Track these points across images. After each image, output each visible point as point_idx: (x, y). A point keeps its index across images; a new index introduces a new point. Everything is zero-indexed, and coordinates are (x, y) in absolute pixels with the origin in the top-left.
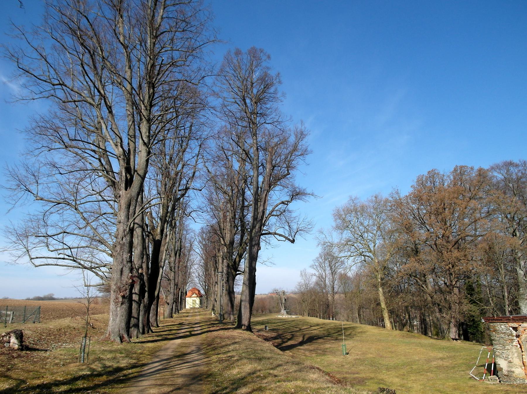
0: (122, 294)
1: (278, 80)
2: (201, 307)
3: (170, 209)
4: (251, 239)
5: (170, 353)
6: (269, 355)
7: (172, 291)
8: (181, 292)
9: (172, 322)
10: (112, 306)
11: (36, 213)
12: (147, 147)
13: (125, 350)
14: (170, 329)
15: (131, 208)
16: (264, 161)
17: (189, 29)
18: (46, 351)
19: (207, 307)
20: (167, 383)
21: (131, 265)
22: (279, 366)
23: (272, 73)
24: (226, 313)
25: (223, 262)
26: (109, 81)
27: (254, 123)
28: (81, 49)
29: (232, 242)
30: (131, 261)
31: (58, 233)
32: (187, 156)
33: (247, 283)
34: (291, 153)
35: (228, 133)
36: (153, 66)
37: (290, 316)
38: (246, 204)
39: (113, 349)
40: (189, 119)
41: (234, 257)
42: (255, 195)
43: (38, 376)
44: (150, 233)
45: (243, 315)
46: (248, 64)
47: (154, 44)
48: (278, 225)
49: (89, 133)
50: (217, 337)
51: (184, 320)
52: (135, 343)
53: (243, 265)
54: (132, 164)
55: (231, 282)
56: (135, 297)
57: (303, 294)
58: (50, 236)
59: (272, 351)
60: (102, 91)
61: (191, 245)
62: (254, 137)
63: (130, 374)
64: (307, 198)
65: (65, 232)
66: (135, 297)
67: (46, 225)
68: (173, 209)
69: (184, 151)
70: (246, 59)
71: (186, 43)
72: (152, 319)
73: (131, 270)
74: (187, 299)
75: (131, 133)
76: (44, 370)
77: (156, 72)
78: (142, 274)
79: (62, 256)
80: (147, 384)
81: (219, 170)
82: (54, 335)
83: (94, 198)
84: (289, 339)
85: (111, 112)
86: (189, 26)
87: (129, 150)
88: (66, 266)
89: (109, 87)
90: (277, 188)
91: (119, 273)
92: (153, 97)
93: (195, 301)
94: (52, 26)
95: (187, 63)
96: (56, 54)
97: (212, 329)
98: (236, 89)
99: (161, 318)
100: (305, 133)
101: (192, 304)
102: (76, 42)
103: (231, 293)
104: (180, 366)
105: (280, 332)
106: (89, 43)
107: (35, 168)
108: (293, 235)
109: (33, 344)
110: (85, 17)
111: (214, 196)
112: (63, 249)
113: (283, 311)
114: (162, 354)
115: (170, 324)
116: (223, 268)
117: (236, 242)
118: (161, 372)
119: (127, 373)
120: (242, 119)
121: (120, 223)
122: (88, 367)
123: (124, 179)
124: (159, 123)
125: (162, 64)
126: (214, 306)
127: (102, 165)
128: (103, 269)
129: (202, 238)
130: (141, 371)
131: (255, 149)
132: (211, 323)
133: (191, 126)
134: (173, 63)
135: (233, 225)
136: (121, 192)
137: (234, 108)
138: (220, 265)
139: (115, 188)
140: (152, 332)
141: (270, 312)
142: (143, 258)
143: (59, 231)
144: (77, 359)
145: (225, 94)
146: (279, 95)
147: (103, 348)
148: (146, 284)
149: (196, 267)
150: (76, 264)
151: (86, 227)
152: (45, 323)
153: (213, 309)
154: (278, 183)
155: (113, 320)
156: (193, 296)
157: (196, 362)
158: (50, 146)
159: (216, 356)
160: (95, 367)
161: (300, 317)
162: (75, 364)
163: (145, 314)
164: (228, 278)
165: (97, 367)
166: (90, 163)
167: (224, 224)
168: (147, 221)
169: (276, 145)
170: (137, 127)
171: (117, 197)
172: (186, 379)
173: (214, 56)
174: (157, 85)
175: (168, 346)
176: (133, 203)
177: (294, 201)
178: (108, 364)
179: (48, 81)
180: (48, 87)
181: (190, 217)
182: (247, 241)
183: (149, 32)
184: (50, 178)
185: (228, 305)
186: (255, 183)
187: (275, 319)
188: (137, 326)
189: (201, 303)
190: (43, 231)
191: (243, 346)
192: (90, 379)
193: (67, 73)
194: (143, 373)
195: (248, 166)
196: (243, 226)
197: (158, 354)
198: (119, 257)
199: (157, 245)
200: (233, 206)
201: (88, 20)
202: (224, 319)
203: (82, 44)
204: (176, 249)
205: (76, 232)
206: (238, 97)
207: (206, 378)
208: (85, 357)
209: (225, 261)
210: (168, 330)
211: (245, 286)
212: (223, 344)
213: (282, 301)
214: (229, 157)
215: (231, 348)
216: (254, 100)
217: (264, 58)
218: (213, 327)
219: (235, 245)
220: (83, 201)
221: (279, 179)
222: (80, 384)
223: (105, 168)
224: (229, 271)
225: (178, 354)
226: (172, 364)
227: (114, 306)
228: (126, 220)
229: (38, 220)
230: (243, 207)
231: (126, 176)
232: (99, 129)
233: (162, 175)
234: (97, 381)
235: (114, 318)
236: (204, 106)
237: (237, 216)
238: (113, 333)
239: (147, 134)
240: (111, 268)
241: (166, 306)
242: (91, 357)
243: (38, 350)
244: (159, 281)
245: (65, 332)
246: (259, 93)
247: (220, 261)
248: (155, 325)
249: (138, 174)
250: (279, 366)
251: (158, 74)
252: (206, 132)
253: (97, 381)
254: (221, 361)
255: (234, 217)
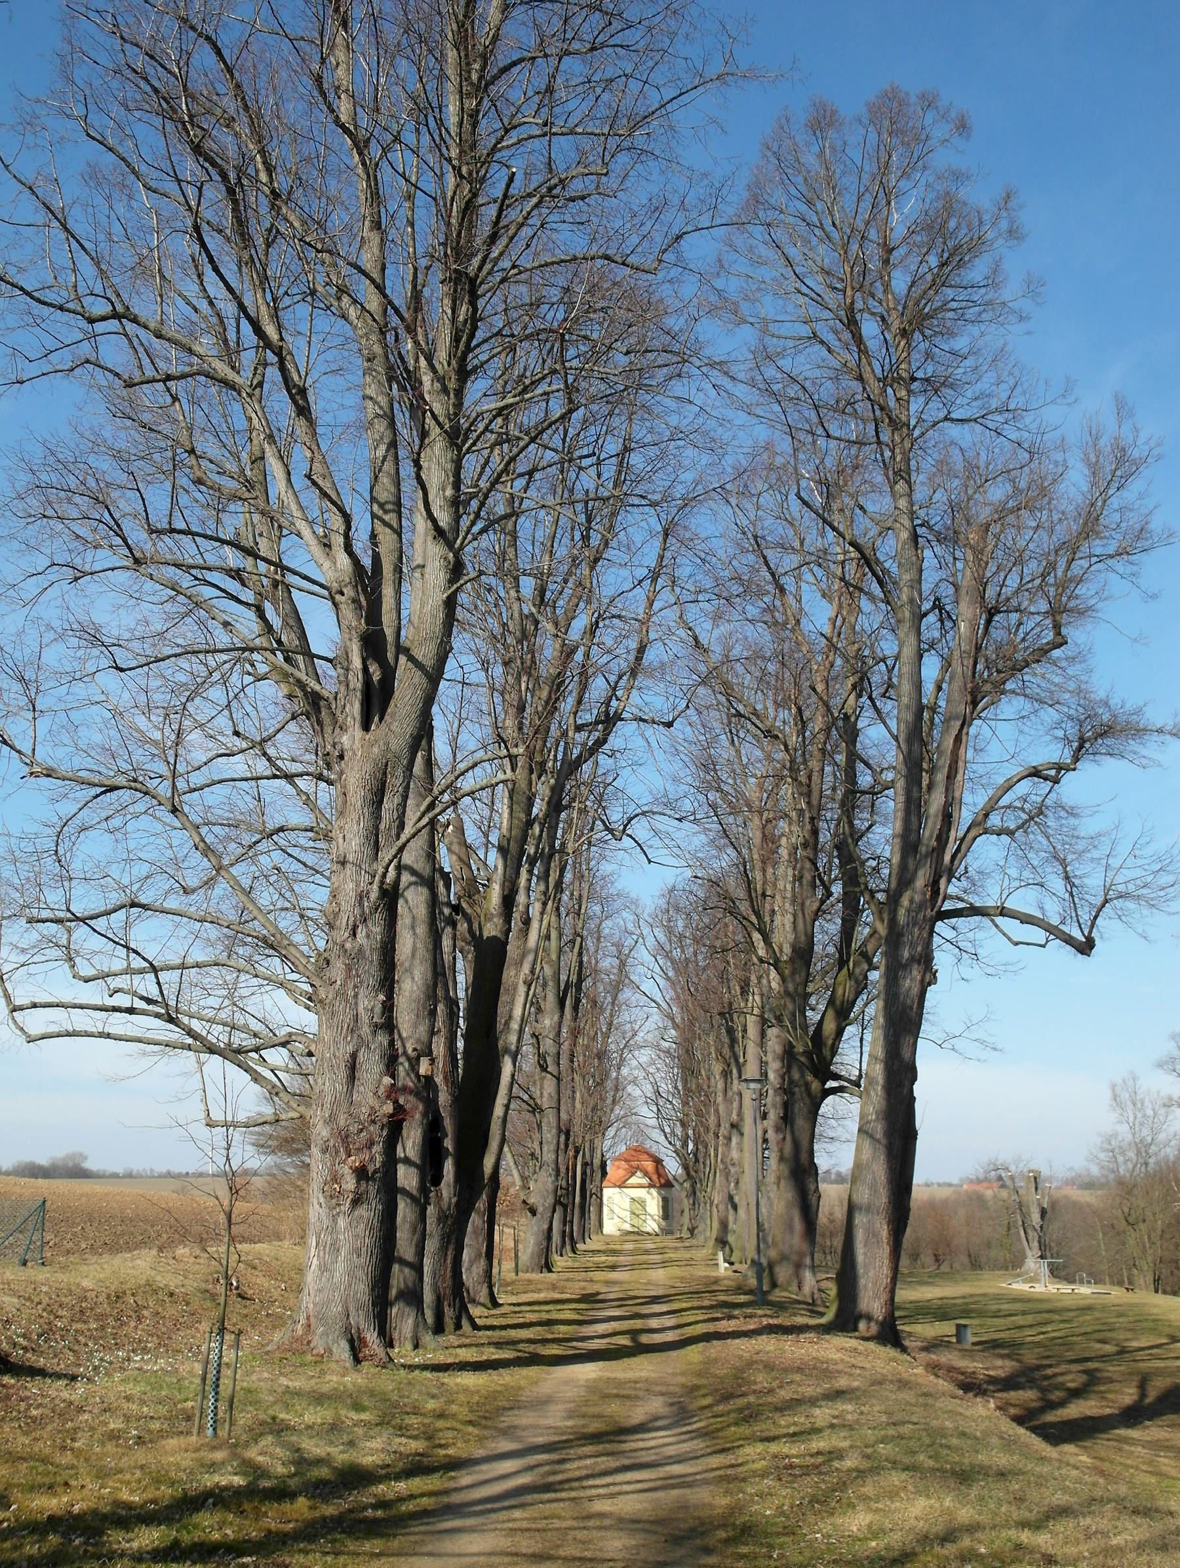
0: (356, 1161)
1: (1004, 225)
2: (667, 1231)
3: (539, 808)
4: (894, 939)
5: (554, 1421)
6: (1002, 1460)
7: (548, 1156)
8: (585, 1164)
9: (554, 1287)
10: (316, 1210)
11: (31, 828)
12: (450, 545)
13: (372, 1393)
14: (545, 1316)
15: (385, 805)
16: (947, 591)
17: (616, 40)
18: (74, 1378)
19: (692, 1231)
20: (561, 1553)
21: (392, 1043)
22: (1064, 1512)
23: (979, 196)
24: (784, 1258)
25: (763, 1034)
26: (295, 290)
27: (896, 425)
28: (190, 167)
29: (804, 953)
30: (388, 1025)
31: (110, 907)
32: (613, 579)
33: (879, 1129)
34: (1072, 549)
35: (781, 477)
36: (470, 208)
37: (1066, 1288)
38: (865, 779)
39: (325, 1388)
40: (616, 421)
41: (813, 1017)
42: (909, 741)
43: (47, 1480)
44: (457, 909)
45: (861, 1271)
46: (870, 167)
47: (474, 116)
48: (1013, 872)
49: (221, 501)
50: (750, 1363)
51: (598, 1282)
52: (411, 1368)
53: (858, 1052)
54: (388, 620)
55: (801, 1123)
56: (407, 1177)
57: (1126, 1188)
58: (83, 920)
59: (1009, 1444)
60: (271, 331)
61: (623, 964)
62: (901, 486)
63: (401, 1499)
64: (1151, 748)
65: (133, 905)
66: (407, 1177)
67: (66, 878)
68: (556, 806)
69: (596, 560)
70: (857, 143)
71: (606, 97)
72: (471, 1275)
73: (391, 1062)
74: (608, 1193)
75: (385, 492)
76: (67, 1459)
77: (484, 230)
78: (429, 1079)
79: (123, 1001)
80: (474, 1549)
81: (740, 633)
82: (100, 1317)
83: (238, 766)
84: (1076, 1394)
85: (303, 411)
86: (617, 25)
87: (376, 559)
88: (139, 1041)
89: (298, 314)
90: (1009, 707)
91: (343, 1073)
92: (472, 336)
93: (642, 1203)
94: (87, 92)
95: (612, 182)
96: (99, 200)
97: (724, 1326)
98: (816, 282)
99: (504, 1269)
100: (1136, 454)
101: (626, 1215)
102: (174, 139)
103: (802, 1172)
104: (609, 1479)
105: (1030, 1358)
106: (224, 142)
107: (27, 651)
108: (1085, 917)
109: (25, 1349)
110: (208, 38)
111: (723, 751)
112: (129, 971)
113: (1032, 1263)
114: (524, 1421)
115: (542, 1296)
116: (763, 1064)
117: (817, 948)
118: (529, 1498)
119: (391, 1496)
120: (845, 407)
121: (343, 863)
122: (234, 1455)
123: (356, 682)
124: (492, 448)
125: (505, 196)
126: (724, 1225)
127: (269, 628)
128: (277, 1057)
129: (669, 931)
130: (446, 1492)
131: (904, 535)
132: (721, 1303)
133: (627, 449)
134: (550, 189)
135: (808, 876)
136: (345, 739)
137: (808, 363)
138: (752, 1050)
139: (320, 723)
140: (475, 1327)
141: (976, 1264)
142: (433, 1013)
143: (115, 898)
144: (189, 1418)
145: (768, 307)
146: (1010, 291)
147: (284, 1381)
148: (448, 1124)
149: (644, 1059)
150: (173, 1034)
151: (209, 883)
152: (64, 1268)
153: (722, 1242)
154: (1009, 686)
155: (324, 1268)
156: (633, 1180)
157: (677, 1469)
158: (78, 562)
159: (760, 1447)
160: (260, 1459)
161: (1117, 1294)
162: (182, 1441)
163: (443, 1248)
164: (787, 1106)
165: (271, 1456)
166: (226, 624)
167: (764, 871)
168: (446, 861)
169: (1002, 513)
170: (407, 469)
171: (330, 763)
172: (639, 1539)
173: (714, 144)
174: (484, 287)
175: (545, 1389)
176: (395, 782)
177: (1084, 765)
178: (314, 1448)
179: (71, 306)
180: (70, 328)
181: (627, 842)
182: (870, 948)
183: (451, 71)
184: (79, 689)
185: (790, 1228)
186: (906, 687)
187: (998, 1298)
188: (413, 1297)
189: (666, 1213)
190: (54, 897)
191: (875, 1410)
192: (247, 1506)
193: (140, 269)
194: (457, 1498)
195: (871, 615)
196: (853, 877)
197: (507, 1420)
198: (339, 1006)
199: (490, 959)
200: (809, 794)
201: (219, 52)
202: (774, 1285)
203: (197, 150)
204: (563, 978)
205: (172, 903)
206: (826, 314)
207: (727, 1541)
208: (221, 1414)
209: (772, 1032)
210: (540, 1324)
211: (867, 1144)
212: (785, 1394)
213: (1024, 1216)
214: (788, 582)
215: (822, 1414)
216: (898, 318)
217: (940, 131)
218: (730, 1317)
219: (817, 966)
220: (197, 779)
221: (1018, 668)
222: (211, 1526)
223: (279, 642)
224: (796, 1075)
225: (594, 1426)
226: (574, 1468)
227: (323, 1212)
228: (368, 851)
229: (38, 855)
230: (851, 798)
231: (365, 670)
232: (254, 486)
233: (506, 664)
234: (274, 1518)
235: (324, 1258)
236: (681, 357)
237: (825, 837)
238: (322, 1319)
239: (449, 492)
240: (310, 1054)
241: (525, 1219)
242: (244, 1418)
243: (42, 1373)
244: (498, 1111)
245: (138, 1308)
246: (917, 292)
247: (753, 1032)
248: (483, 1296)
249: (411, 658)
250: (1064, 1512)
251: (493, 238)
252: (691, 467)
253: (274, 1518)
254: (785, 1471)
255: (812, 843)
